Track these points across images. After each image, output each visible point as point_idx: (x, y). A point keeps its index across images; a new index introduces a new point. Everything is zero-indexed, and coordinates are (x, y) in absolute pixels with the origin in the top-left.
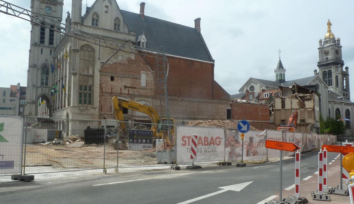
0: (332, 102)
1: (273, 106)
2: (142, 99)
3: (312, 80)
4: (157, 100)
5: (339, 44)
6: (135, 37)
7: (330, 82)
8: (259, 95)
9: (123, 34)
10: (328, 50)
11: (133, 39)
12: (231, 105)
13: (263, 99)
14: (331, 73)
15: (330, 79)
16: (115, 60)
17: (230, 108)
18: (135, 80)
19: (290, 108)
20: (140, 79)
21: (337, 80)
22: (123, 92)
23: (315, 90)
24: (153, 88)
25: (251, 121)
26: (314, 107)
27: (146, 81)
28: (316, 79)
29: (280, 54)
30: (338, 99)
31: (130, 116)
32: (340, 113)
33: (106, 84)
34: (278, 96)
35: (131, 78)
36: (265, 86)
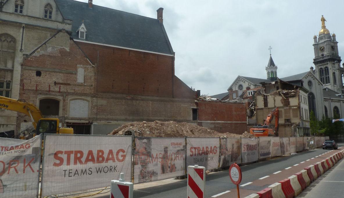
0: (329, 100)
1: (255, 105)
2: (79, 97)
3: (304, 76)
4: (99, 99)
5: (334, 39)
6: (71, 25)
7: (328, 80)
8: (243, 93)
9: (55, 22)
10: (324, 46)
11: (68, 28)
12: (196, 103)
13: (247, 98)
14: (328, 70)
15: (327, 76)
16: (42, 52)
17: (195, 107)
18: (70, 75)
19: (273, 106)
20: (76, 74)
21: (335, 77)
22: (52, 89)
23: (300, 86)
24: (93, 85)
25: (223, 122)
26: (299, 104)
27: (84, 77)
28: (308, 76)
29: (270, 51)
30: (336, 97)
31: (61, 118)
32: (339, 112)
33: (29, 80)
34: (259, 94)
35: (63, 73)
36: (253, 84)
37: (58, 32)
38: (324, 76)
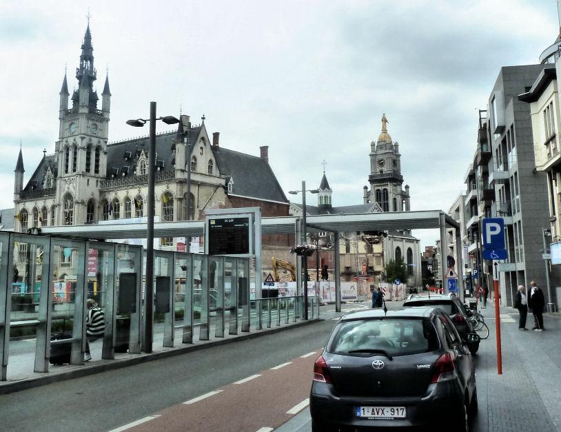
5: (396, 151)
14: (387, 193)
37: (217, 188)
38: (382, 202)
